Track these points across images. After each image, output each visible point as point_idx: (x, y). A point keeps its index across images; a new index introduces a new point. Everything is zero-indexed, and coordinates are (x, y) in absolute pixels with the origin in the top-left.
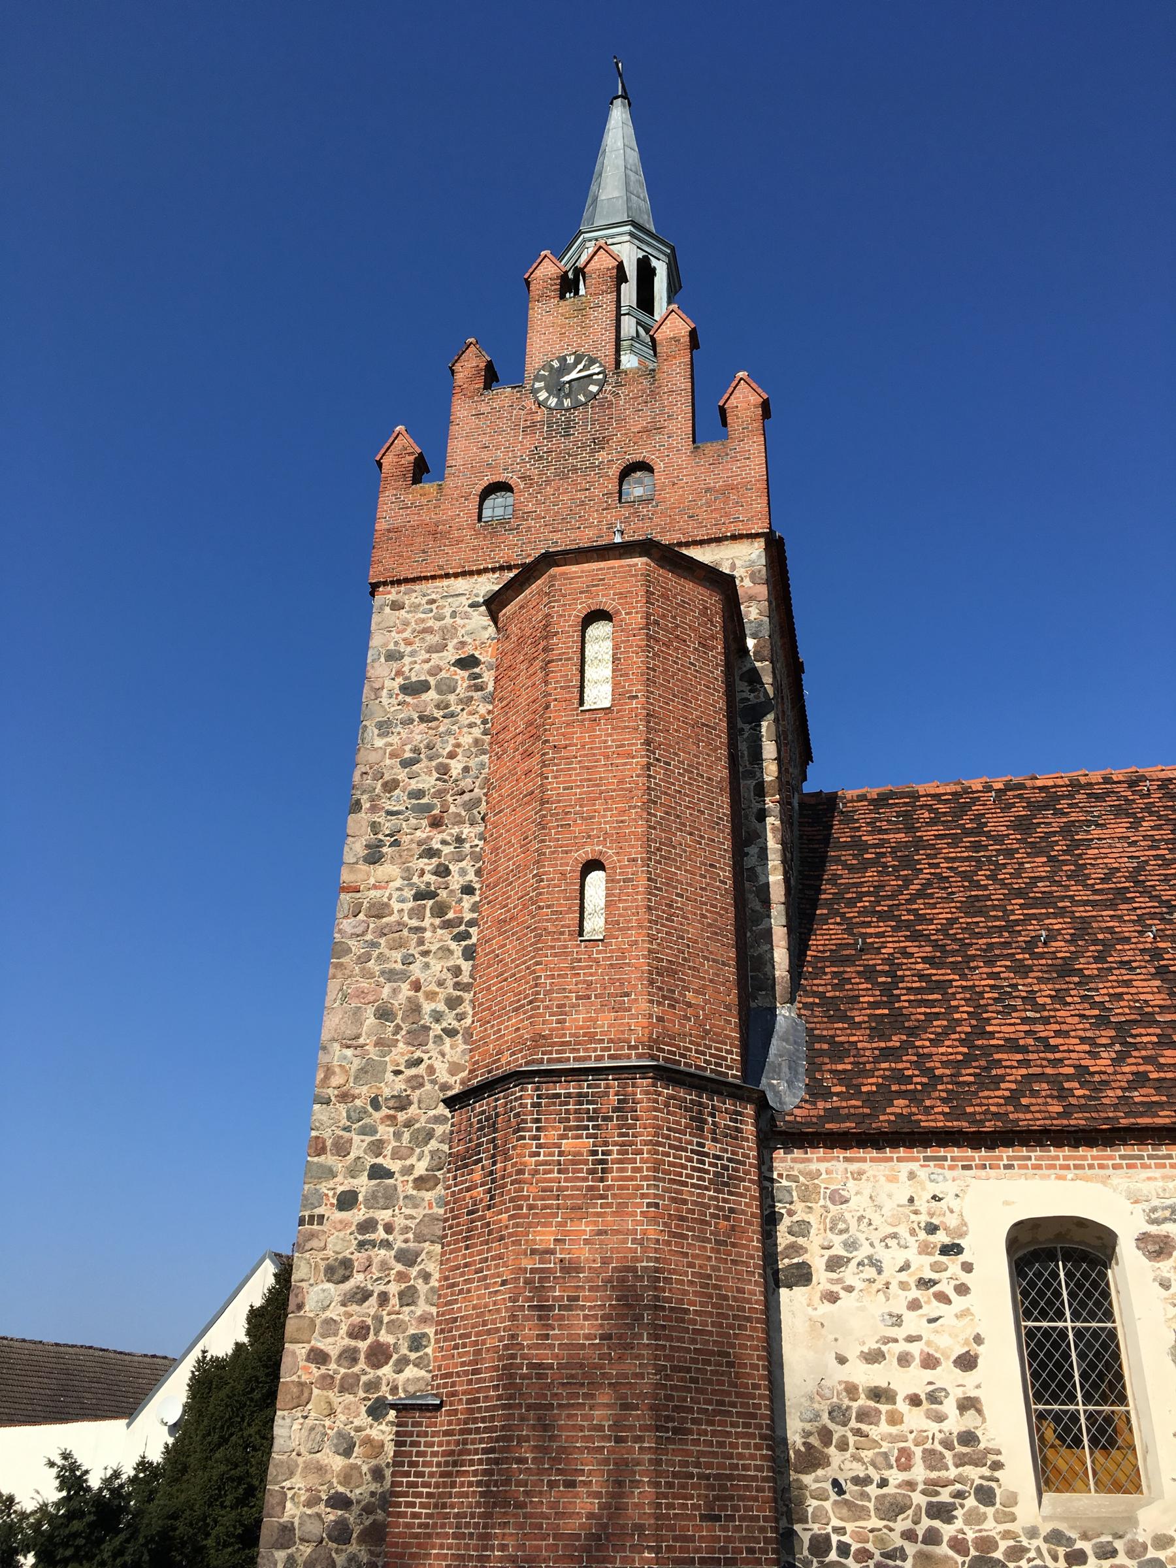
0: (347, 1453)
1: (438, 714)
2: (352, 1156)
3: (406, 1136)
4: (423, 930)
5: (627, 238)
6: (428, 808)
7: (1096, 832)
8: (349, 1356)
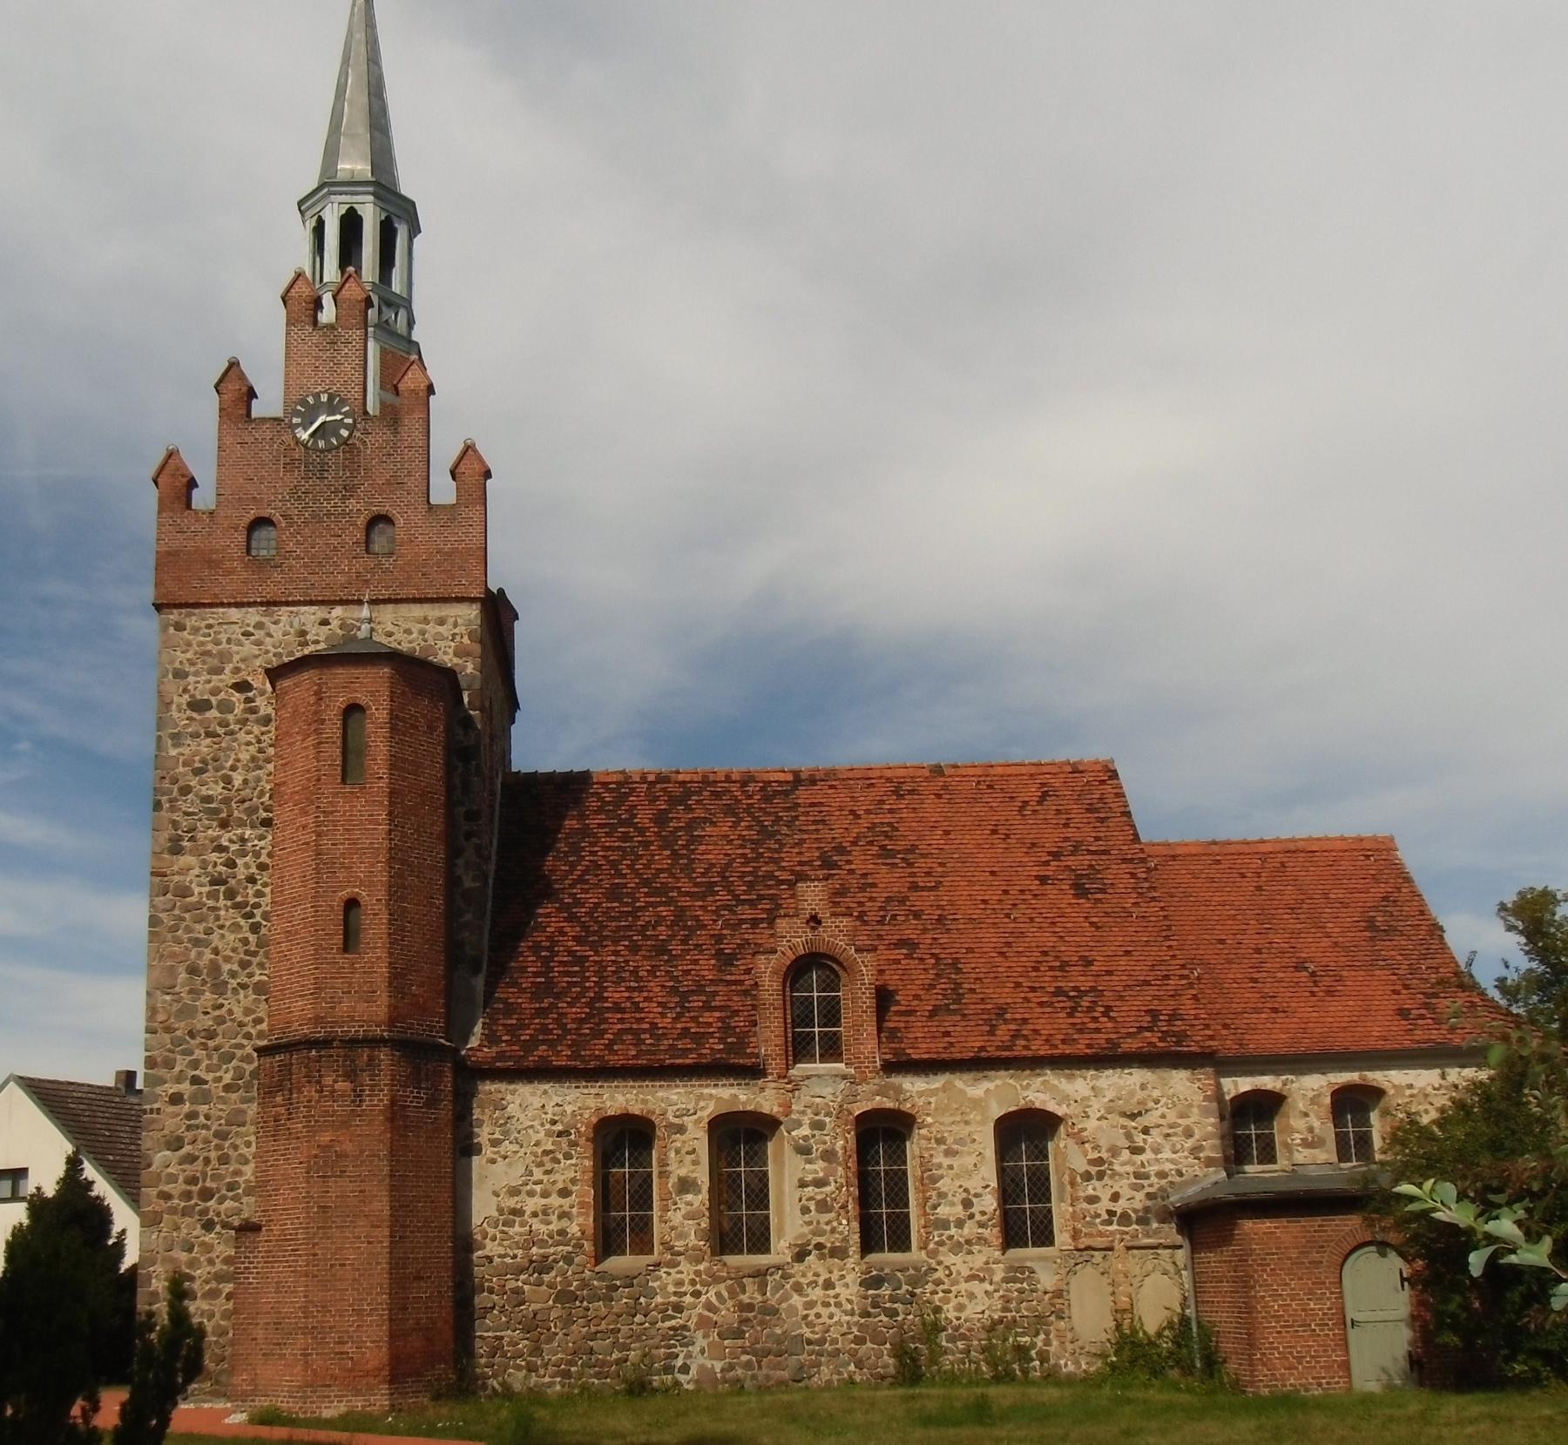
0: (190, 1250)
1: (221, 731)
2: (177, 1069)
3: (215, 1057)
4: (218, 909)
5: (371, 198)
6: (216, 811)
7: (709, 829)
8: (187, 1195)
